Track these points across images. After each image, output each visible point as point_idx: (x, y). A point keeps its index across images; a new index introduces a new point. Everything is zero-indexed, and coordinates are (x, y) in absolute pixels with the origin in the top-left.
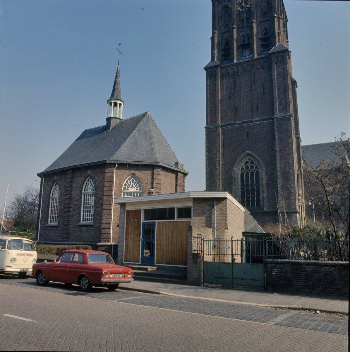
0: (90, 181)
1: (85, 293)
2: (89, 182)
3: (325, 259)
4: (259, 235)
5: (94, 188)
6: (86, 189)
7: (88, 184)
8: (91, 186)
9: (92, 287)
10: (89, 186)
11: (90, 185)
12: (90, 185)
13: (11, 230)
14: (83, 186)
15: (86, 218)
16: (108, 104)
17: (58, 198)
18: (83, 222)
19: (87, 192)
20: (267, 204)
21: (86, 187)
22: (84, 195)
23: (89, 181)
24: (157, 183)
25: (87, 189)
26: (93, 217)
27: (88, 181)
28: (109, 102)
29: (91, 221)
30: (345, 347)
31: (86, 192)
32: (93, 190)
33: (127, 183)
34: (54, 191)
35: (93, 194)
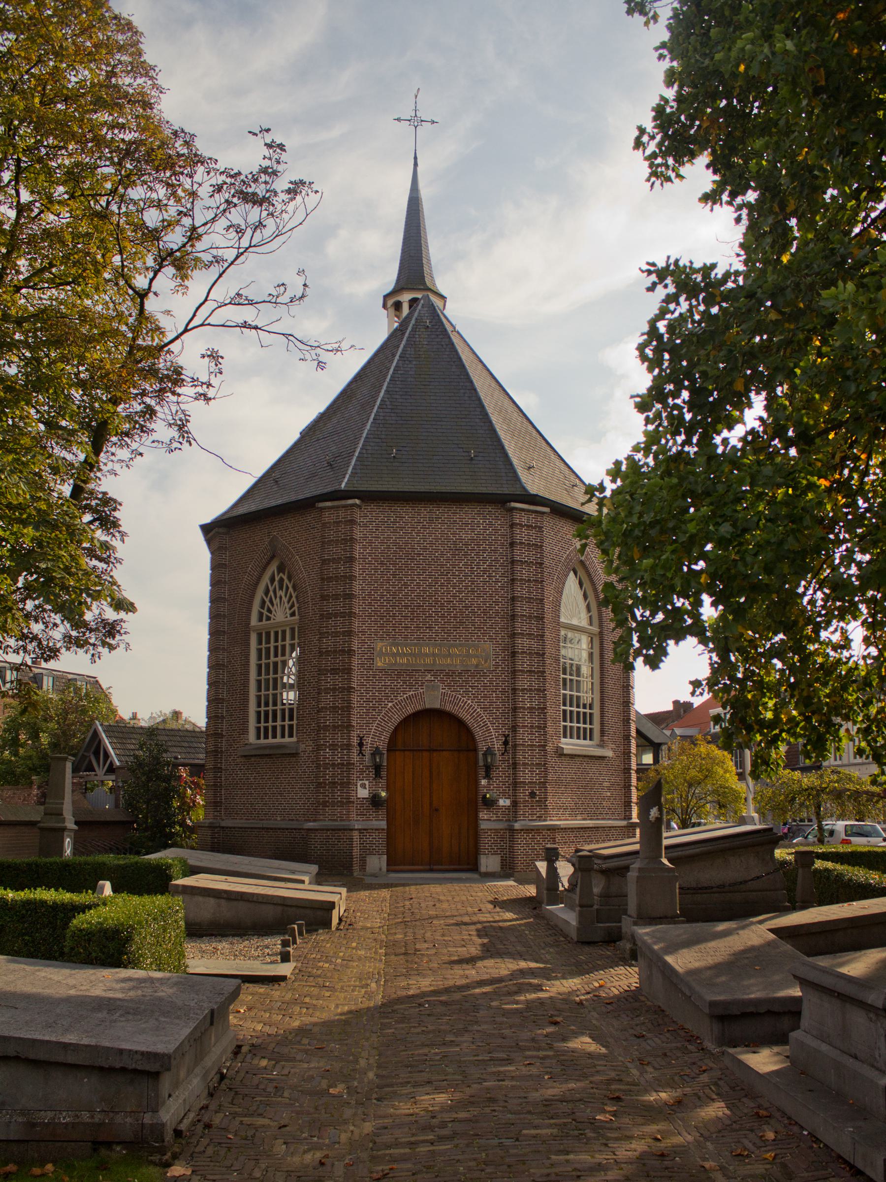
0: (281, 581)
2: (276, 583)
3: (434, 661)
4: (397, 868)
6: (265, 612)
7: (271, 593)
9: (544, 874)
10: (276, 601)
11: (278, 596)
12: (281, 598)
13: (297, 725)
15: (287, 723)
16: (386, 312)
17: (293, 630)
18: (259, 742)
19: (268, 622)
20: (202, 803)
22: (260, 636)
23: (277, 579)
25: (269, 611)
26: (295, 722)
27: (272, 580)
28: (390, 302)
29: (291, 735)
31: (264, 622)
32: (293, 614)
33: (267, 597)
34: (268, 603)
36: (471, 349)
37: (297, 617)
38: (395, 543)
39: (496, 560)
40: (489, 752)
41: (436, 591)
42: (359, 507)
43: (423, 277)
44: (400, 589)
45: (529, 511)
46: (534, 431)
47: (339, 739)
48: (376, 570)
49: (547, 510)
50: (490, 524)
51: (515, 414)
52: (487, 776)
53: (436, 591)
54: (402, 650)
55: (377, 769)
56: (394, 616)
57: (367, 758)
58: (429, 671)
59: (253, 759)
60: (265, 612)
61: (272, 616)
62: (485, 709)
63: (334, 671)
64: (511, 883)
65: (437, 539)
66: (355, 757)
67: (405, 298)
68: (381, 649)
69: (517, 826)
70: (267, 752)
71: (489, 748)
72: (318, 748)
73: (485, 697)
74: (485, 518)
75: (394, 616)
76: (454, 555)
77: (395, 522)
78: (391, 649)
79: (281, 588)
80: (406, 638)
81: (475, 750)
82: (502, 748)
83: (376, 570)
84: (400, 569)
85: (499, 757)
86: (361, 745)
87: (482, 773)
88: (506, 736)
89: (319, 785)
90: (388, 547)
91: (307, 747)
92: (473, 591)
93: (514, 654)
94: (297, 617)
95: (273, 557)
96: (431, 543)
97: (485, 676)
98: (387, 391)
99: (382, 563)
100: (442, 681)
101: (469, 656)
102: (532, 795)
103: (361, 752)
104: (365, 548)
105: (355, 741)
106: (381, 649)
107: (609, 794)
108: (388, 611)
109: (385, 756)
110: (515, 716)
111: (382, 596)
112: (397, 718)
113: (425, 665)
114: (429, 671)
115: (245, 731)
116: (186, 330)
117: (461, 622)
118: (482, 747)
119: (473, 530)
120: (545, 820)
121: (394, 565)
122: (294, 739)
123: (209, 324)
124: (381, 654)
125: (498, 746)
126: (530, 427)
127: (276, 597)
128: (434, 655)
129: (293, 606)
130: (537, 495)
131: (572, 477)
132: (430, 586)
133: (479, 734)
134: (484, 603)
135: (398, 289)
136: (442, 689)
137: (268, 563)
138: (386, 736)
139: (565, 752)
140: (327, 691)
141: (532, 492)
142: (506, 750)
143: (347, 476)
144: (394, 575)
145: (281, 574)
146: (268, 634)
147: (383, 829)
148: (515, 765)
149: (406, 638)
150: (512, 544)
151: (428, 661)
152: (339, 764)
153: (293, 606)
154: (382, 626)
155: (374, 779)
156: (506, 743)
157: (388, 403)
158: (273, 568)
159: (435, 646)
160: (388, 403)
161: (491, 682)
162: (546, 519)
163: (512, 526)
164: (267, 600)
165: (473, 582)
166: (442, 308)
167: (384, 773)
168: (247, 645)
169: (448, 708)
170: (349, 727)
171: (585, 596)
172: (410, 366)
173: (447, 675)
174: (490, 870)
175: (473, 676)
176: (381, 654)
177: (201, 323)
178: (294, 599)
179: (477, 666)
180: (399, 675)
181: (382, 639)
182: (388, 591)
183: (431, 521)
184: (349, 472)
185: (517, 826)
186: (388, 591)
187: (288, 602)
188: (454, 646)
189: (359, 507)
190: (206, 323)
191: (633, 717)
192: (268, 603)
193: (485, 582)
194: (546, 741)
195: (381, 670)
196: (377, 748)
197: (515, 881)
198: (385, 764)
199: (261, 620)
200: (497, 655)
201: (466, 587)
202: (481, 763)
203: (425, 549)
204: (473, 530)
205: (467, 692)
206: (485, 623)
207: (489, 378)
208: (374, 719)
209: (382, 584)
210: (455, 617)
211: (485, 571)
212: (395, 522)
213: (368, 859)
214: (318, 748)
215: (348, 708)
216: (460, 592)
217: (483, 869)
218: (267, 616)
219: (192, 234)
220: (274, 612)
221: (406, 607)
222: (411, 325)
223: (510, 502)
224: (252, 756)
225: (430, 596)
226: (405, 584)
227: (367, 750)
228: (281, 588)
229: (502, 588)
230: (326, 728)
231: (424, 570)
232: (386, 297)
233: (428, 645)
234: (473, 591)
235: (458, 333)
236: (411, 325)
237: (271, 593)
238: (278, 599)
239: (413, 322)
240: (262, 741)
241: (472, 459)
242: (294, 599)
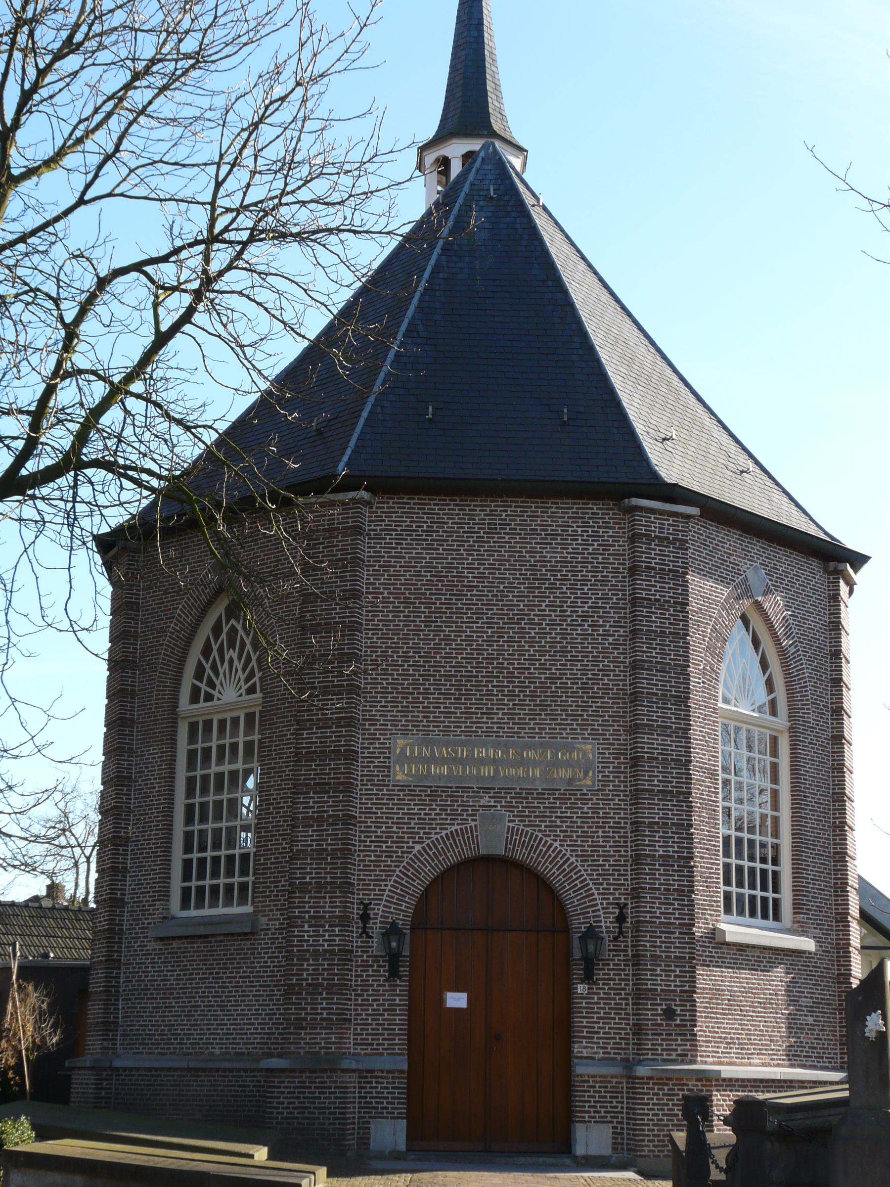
0: (233, 630)
1: (514, 175)
3: (496, 771)
5: (258, 675)
6: (203, 687)
7: (215, 653)
8: (236, 662)
10: (223, 669)
11: (227, 658)
12: (231, 661)
13: (254, 883)
14: (788, 684)
21: (199, 673)
22: (193, 727)
24: (108, 158)
27: (217, 630)
28: (430, 158)
29: (243, 901)
30: (237, 345)
32: (251, 690)
34: (208, 671)
35: (250, 717)
36: (567, 237)
37: (259, 695)
38: (430, 567)
39: (605, 598)
40: (591, 933)
41: (500, 650)
42: (368, 503)
43: (488, 115)
44: (437, 648)
45: (662, 512)
46: (675, 378)
47: (329, 906)
48: (396, 612)
49: (694, 511)
50: (596, 536)
51: (643, 349)
52: (588, 977)
53: (500, 650)
54: (440, 752)
55: (393, 960)
56: (426, 692)
57: (375, 942)
58: (486, 790)
59: (175, 944)
60: (203, 687)
61: (215, 693)
62: (584, 858)
63: (321, 788)
64: (630, 1175)
65: (502, 562)
66: (356, 942)
67: (456, 150)
68: (403, 750)
69: (642, 1071)
70: (202, 931)
71: (590, 928)
72: (291, 923)
73: (585, 836)
74: (585, 524)
75: (426, 692)
76: (531, 589)
77: (430, 531)
78: (421, 750)
79: (232, 645)
80: (446, 731)
81: (566, 930)
82: (613, 927)
83: (396, 612)
84: (438, 611)
85: (608, 945)
86: (365, 917)
87: (578, 971)
88: (622, 907)
89: (290, 990)
90: (418, 575)
91: (271, 922)
92: (564, 652)
93: (635, 762)
94: (259, 695)
95: (219, 592)
96: (492, 568)
97: (584, 798)
98: (419, 308)
99: (407, 602)
100: (509, 807)
101: (556, 763)
102: (669, 1014)
103: (364, 932)
104: (377, 575)
105: (356, 911)
106: (403, 750)
107: (810, 1020)
108: (415, 683)
109: (408, 937)
110: (637, 871)
111: (406, 658)
112: (428, 873)
113: (479, 778)
114: (486, 790)
115: (166, 895)
116: (81, 201)
117: (543, 706)
118: (579, 925)
119: (565, 546)
120: (693, 1062)
121: (428, 605)
122: (248, 909)
123: (122, 195)
124: (403, 759)
125: (606, 923)
126: (669, 371)
127: (222, 661)
128: (495, 762)
129: (251, 675)
130: (676, 485)
131: (742, 458)
132: (490, 641)
133: (572, 901)
134: (584, 672)
135: (444, 135)
136: (508, 821)
137: (210, 603)
138: (407, 905)
139: (728, 939)
140: (307, 822)
141: (668, 481)
142: (621, 932)
143: (349, 452)
144: (428, 623)
145: (233, 622)
146: (208, 724)
147: (401, 1072)
148: (637, 960)
149: (446, 731)
150: (633, 571)
151: (487, 771)
152: (325, 951)
153: (251, 675)
154: (405, 711)
155: (387, 980)
156: (621, 919)
157: (421, 328)
158: (219, 609)
159: (496, 746)
160: (421, 328)
161: (595, 810)
162: (694, 527)
163: (634, 538)
164: (207, 666)
165: (564, 635)
166: (518, 168)
167: (404, 970)
168: (174, 743)
169: (520, 854)
170: (346, 887)
171: (764, 664)
172: (459, 265)
173: (519, 796)
174: (593, 1151)
175: (564, 800)
176: (403, 759)
177: (108, 191)
178: (254, 663)
179: (570, 781)
180: (433, 796)
181: (405, 733)
182: (417, 650)
183: (492, 530)
184: (353, 443)
185: (642, 1071)
186: (417, 650)
187: (244, 670)
188: (529, 747)
189: (368, 503)
190: (117, 191)
191: (852, 881)
192: (208, 671)
193: (585, 636)
194: (692, 917)
195: (403, 787)
196: (394, 924)
197: (635, 1172)
198: (406, 953)
199: (195, 699)
200: (605, 763)
201: (553, 644)
202: (577, 954)
203: (482, 576)
204: (565, 546)
205: (552, 827)
206: (585, 708)
207: (598, 285)
208: (389, 872)
209: (406, 638)
210: (533, 696)
211: (585, 617)
212: (430, 531)
213: (372, 1126)
214: (291, 923)
215: (346, 852)
216: (542, 653)
217: (580, 1150)
218: (206, 693)
219: (117, 447)
220: (218, 687)
221: (448, 677)
222: (462, 195)
223: (629, 497)
224: (174, 938)
225: (490, 659)
226: (447, 638)
227: (376, 927)
228: (232, 645)
229: (615, 645)
230: (304, 888)
231: (480, 613)
232: (424, 149)
233: (484, 745)
234: (564, 652)
235: (544, 208)
236: (462, 195)
237: (215, 653)
238: (226, 664)
239: (466, 189)
240: (193, 913)
241: (564, 424)
242: (254, 663)
